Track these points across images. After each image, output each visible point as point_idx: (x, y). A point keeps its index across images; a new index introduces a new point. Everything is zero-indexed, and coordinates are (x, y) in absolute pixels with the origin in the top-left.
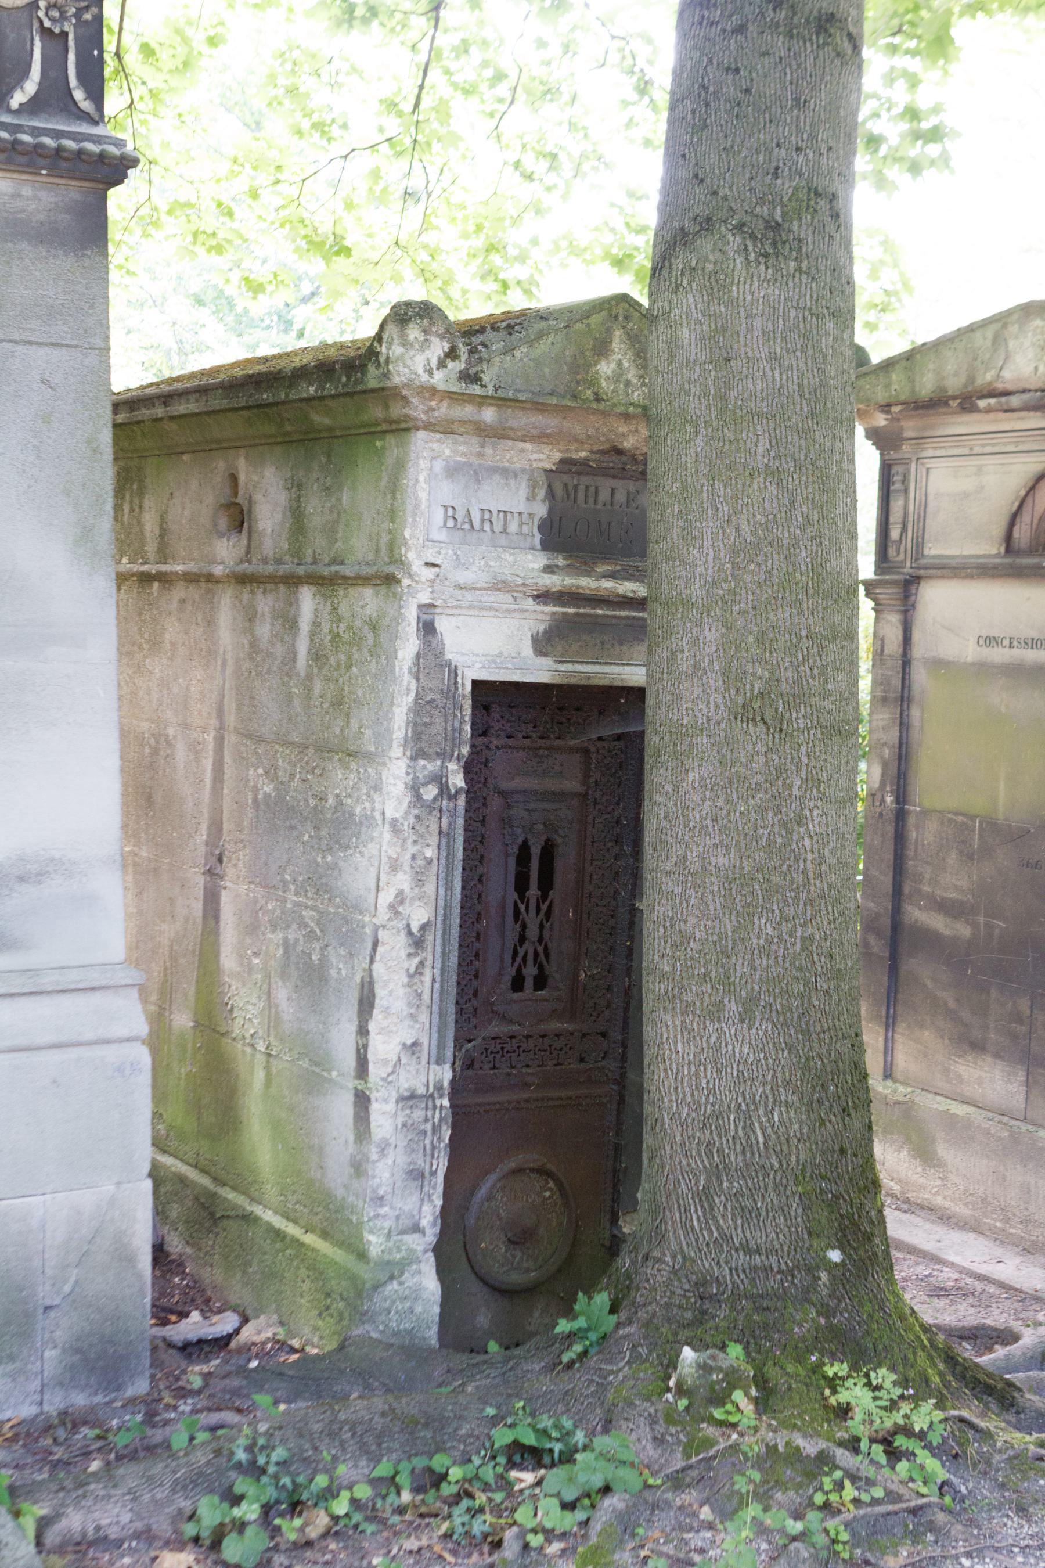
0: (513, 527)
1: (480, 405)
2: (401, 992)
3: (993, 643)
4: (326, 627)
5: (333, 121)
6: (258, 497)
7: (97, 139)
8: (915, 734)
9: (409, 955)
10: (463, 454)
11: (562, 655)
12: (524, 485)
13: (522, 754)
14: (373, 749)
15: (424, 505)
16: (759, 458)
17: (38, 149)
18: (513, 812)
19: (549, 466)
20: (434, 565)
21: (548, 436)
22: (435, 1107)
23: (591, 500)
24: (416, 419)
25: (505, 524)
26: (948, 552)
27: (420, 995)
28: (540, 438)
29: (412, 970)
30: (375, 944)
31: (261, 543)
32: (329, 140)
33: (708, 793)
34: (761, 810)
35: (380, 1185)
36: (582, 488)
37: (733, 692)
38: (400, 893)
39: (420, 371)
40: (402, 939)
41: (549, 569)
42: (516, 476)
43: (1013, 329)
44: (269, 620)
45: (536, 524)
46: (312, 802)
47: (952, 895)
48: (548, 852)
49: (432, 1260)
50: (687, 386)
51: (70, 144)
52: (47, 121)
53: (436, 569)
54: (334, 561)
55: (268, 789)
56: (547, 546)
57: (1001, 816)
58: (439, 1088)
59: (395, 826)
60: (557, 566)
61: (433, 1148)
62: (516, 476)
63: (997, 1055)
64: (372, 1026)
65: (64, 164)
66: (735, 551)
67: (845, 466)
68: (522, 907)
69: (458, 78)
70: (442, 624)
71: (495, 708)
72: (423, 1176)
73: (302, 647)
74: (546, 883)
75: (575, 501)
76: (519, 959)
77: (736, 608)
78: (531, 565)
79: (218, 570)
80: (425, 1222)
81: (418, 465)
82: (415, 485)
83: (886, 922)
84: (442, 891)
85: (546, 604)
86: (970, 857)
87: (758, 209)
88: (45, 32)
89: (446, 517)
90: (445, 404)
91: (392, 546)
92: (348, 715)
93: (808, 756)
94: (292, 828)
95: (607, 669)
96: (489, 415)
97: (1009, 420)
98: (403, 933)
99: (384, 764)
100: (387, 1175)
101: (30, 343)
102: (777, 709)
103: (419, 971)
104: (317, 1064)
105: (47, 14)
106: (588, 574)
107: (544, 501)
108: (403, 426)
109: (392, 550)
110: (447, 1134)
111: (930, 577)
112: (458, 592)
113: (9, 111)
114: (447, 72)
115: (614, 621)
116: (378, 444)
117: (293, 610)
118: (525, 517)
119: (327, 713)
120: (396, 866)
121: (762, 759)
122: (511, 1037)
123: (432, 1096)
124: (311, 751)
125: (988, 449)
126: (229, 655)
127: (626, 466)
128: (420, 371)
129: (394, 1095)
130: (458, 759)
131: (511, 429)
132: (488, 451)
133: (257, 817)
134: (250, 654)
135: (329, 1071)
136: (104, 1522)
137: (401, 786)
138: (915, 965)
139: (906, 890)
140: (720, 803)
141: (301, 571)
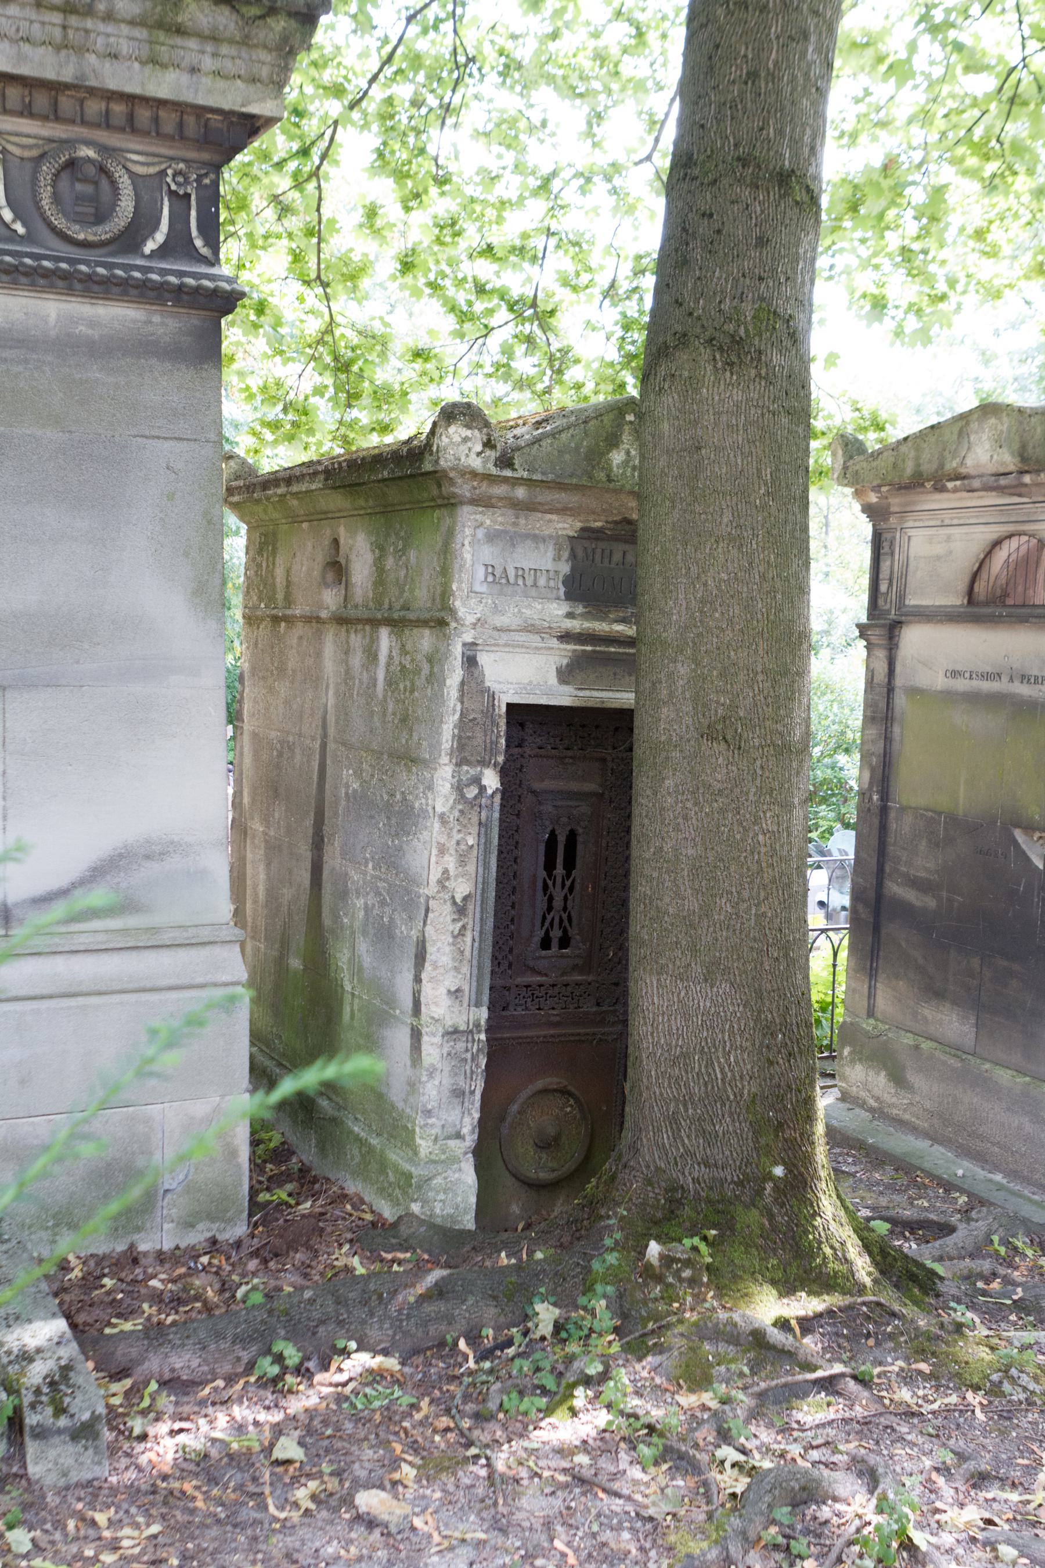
0: (542, 581)
1: (514, 485)
2: (447, 949)
6: (353, 557)
7: (212, 278)
8: (896, 746)
9: (454, 920)
10: (501, 524)
12: (551, 548)
15: (469, 563)
17: (180, 288)
19: (572, 534)
21: (571, 509)
22: (473, 1040)
23: (606, 560)
26: (924, 603)
27: (462, 952)
28: (563, 511)
29: (456, 932)
30: (427, 910)
34: (723, 811)
35: (429, 1100)
36: (599, 551)
38: (446, 871)
40: (448, 908)
41: (570, 615)
43: (974, 426)
46: (386, 797)
47: (922, 874)
48: (572, 838)
49: (472, 1159)
51: (190, 281)
52: (173, 263)
56: (569, 596)
57: (961, 813)
58: (477, 1025)
59: (443, 819)
61: (472, 1072)
63: (955, 1003)
64: (424, 976)
65: (185, 297)
67: (797, 534)
68: (550, 883)
70: (483, 659)
71: (529, 725)
72: (464, 1093)
74: (570, 864)
76: (547, 924)
77: (703, 649)
78: (556, 611)
79: (324, 614)
80: (465, 1131)
83: (872, 894)
84: (481, 870)
85: (568, 643)
86: (937, 845)
87: (726, 327)
88: (172, 193)
93: (762, 767)
94: (372, 817)
95: (618, 695)
96: (521, 492)
98: (449, 903)
100: (435, 1093)
101: (158, 438)
103: (462, 932)
104: (387, 1004)
105: (173, 180)
108: (452, 501)
110: (483, 1061)
111: (910, 622)
112: (496, 633)
113: (143, 256)
118: (552, 574)
120: (444, 851)
122: (540, 986)
123: (471, 1032)
124: (385, 756)
125: (955, 522)
126: (331, 681)
127: (626, 532)
129: (441, 1030)
132: (522, 521)
134: (345, 680)
135: (394, 1009)
136: (177, 1366)
138: (891, 929)
139: (887, 869)
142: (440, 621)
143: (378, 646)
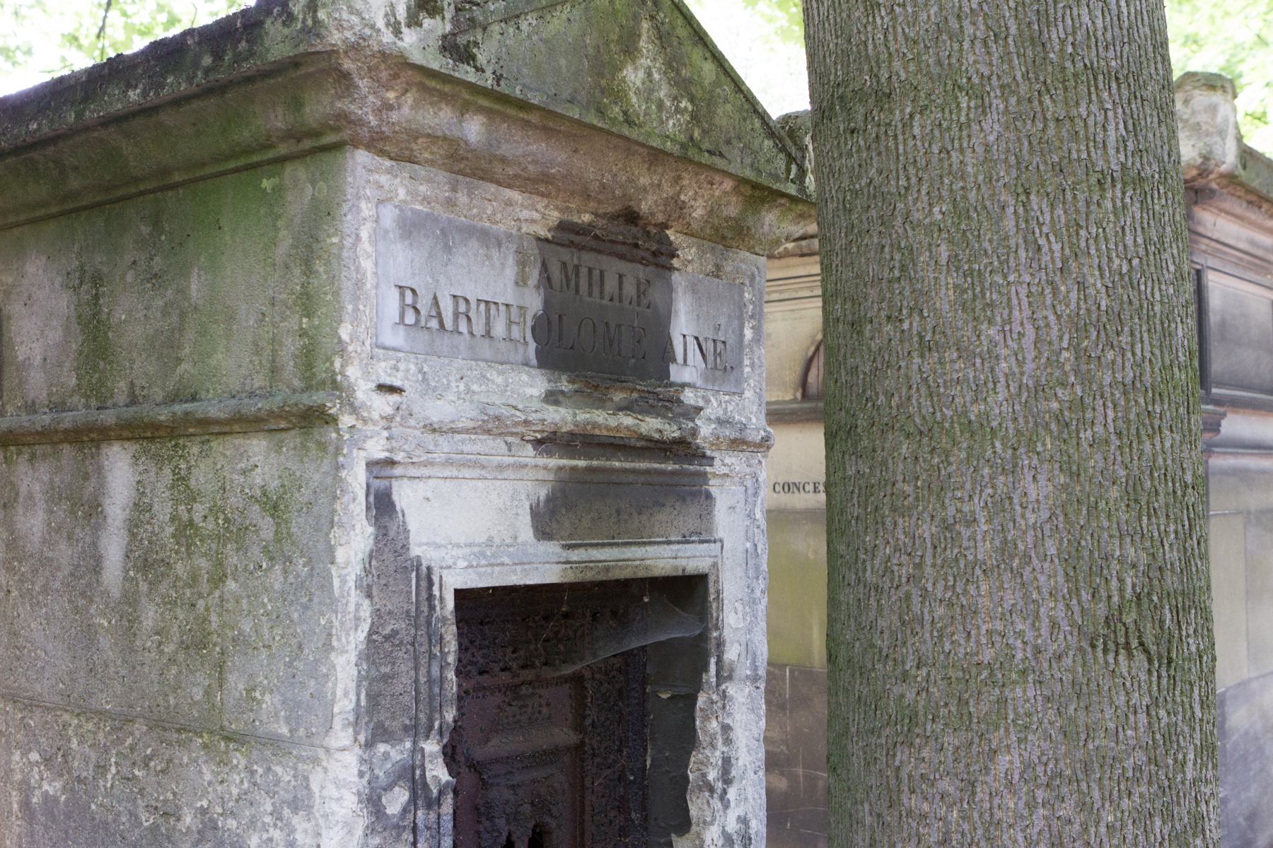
0: (499, 329)
3: (793, 488)
4: (163, 510)
5: (18, 48)
10: (426, 200)
11: (570, 536)
12: (511, 260)
13: (497, 699)
14: (284, 730)
15: (369, 283)
16: (1112, 152)
18: (493, 794)
19: (543, 233)
20: (392, 389)
23: (596, 290)
24: (360, 122)
25: (488, 323)
28: (537, 183)
31: (22, 382)
32: (14, 64)
33: (1040, 794)
37: (1085, 596)
39: (380, 24)
41: (552, 398)
42: (499, 245)
44: (41, 505)
45: (529, 323)
46: (147, 820)
50: (953, 23)
53: (394, 398)
54: (174, 398)
55: (52, 787)
60: (562, 392)
62: (499, 245)
66: (1079, 326)
69: (136, 20)
70: (405, 495)
73: (113, 548)
75: (577, 291)
78: (526, 389)
81: (359, 210)
82: (355, 245)
85: (550, 454)
86: (782, 707)
89: (403, 306)
90: (409, 98)
91: (309, 357)
92: (220, 667)
95: (630, 552)
96: (474, 129)
97: (805, 265)
99: (315, 761)
102: (1162, 622)
106: (601, 403)
107: (537, 287)
109: (309, 366)
112: (429, 437)
114: (124, 14)
115: (631, 478)
116: (266, 184)
117: (90, 487)
118: (514, 311)
119: (173, 661)
121: (1142, 718)
124: (140, 728)
128: (380, 24)
130: (441, 733)
131: (504, 160)
133: (32, 834)
137: (350, 801)
140: (1066, 810)
141: (108, 417)
142: (307, 418)
143: (102, 484)
